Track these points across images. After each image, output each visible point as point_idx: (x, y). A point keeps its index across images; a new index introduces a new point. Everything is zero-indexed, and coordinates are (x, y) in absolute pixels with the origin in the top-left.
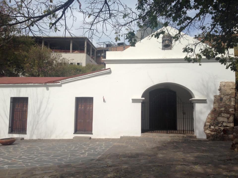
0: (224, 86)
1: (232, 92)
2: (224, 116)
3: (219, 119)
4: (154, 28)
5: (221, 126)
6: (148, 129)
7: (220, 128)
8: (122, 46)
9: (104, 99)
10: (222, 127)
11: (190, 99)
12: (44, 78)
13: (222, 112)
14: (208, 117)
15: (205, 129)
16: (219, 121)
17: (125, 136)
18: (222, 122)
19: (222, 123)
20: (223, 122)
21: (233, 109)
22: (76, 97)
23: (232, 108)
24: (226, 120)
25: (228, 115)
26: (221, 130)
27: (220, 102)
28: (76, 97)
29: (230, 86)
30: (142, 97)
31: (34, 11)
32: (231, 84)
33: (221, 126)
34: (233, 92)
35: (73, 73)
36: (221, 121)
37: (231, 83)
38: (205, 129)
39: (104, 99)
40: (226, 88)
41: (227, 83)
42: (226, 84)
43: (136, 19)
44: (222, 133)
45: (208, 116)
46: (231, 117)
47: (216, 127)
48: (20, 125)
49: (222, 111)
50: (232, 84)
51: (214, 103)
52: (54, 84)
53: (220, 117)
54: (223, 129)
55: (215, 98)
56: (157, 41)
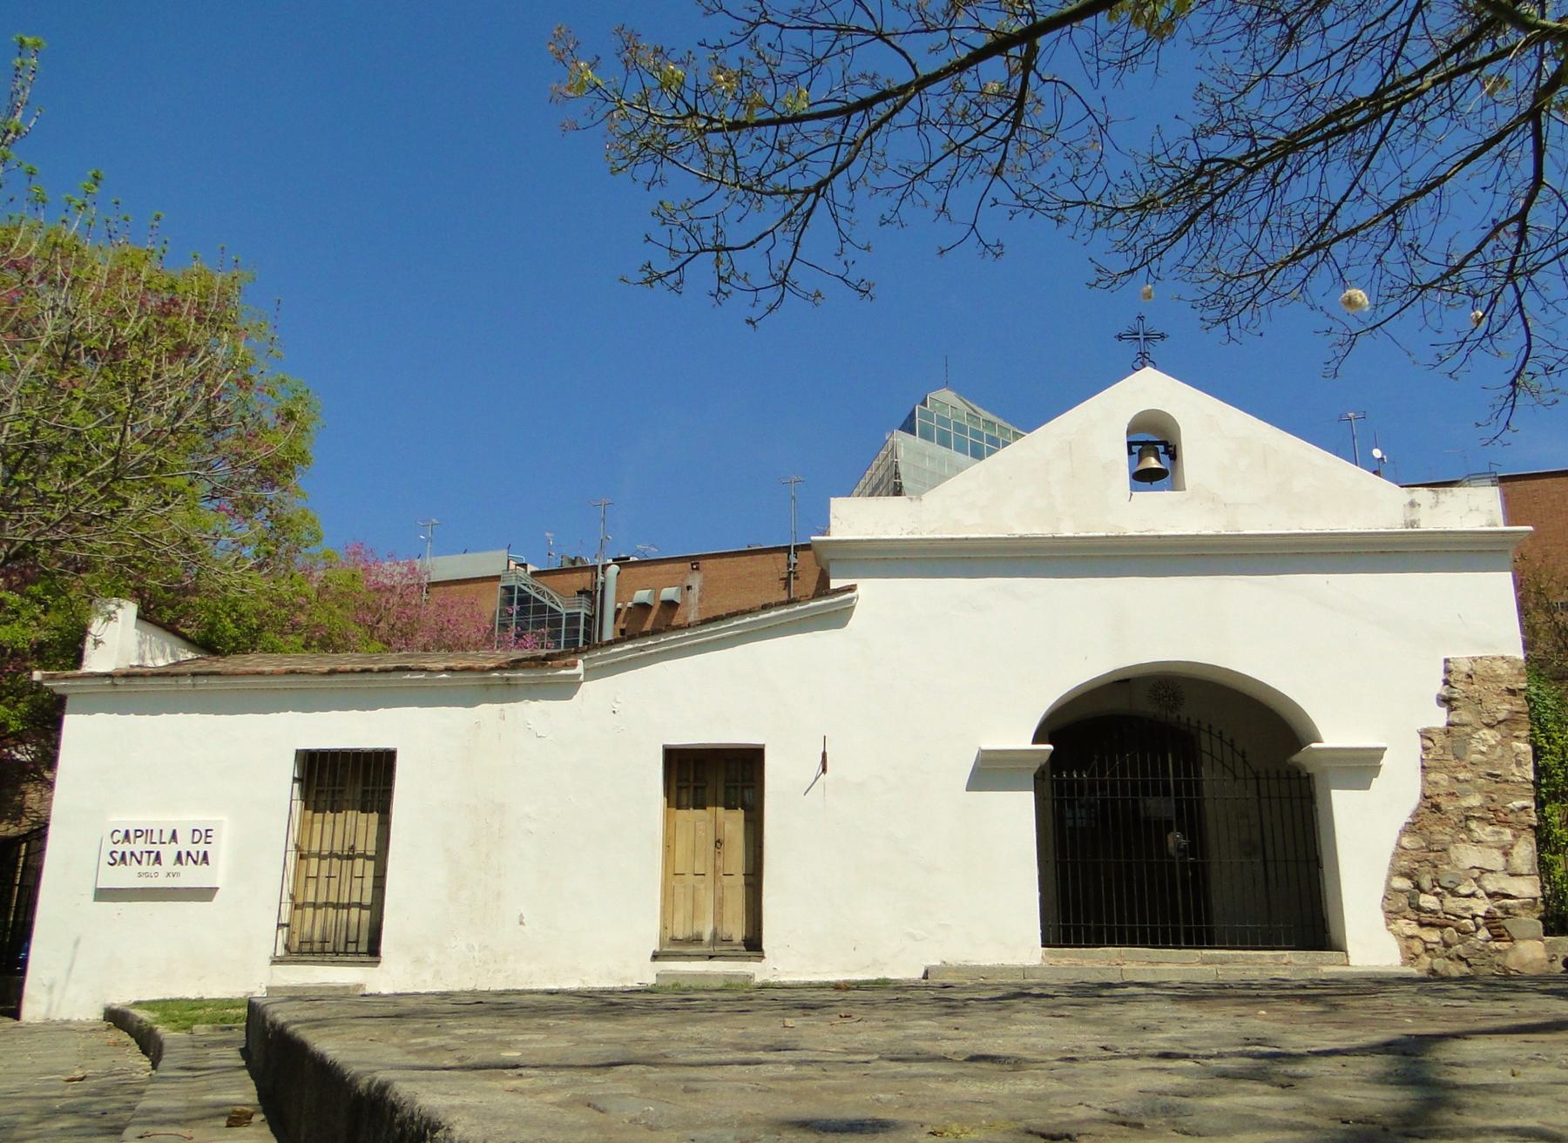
1: (1510, 712)
2: (1484, 837)
5: (1473, 895)
7: (1472, 902)
10: (1481, 902)
11: (1170, 755)
14: (1399, 845)
15: (1390, 912)
20: (1483, 871)
21: (1526, 803)
22: (298, 752)
23: (1523, 797)
24: (1495, 860)
25: (1507, 834)
26: (1474, 917)
28: (298, 752)
29: (1497, 678)
30: (1036, 741)
31: (1328, 28)
32: (1502, 669)
33: (1473, 895)
34: (1515, 708)
35: (262, 598)
37: (1500, 663)
38: (1390, 912)
42: (1478, 668)
44: (1484, 934)
45: (1399, 839)
46: (1521, 842)
48: (1338, 992)
49: (1469, 809)
51: (1423, 767)
52: (620, 649)
54: (1485, 908)
55: (47, 775)
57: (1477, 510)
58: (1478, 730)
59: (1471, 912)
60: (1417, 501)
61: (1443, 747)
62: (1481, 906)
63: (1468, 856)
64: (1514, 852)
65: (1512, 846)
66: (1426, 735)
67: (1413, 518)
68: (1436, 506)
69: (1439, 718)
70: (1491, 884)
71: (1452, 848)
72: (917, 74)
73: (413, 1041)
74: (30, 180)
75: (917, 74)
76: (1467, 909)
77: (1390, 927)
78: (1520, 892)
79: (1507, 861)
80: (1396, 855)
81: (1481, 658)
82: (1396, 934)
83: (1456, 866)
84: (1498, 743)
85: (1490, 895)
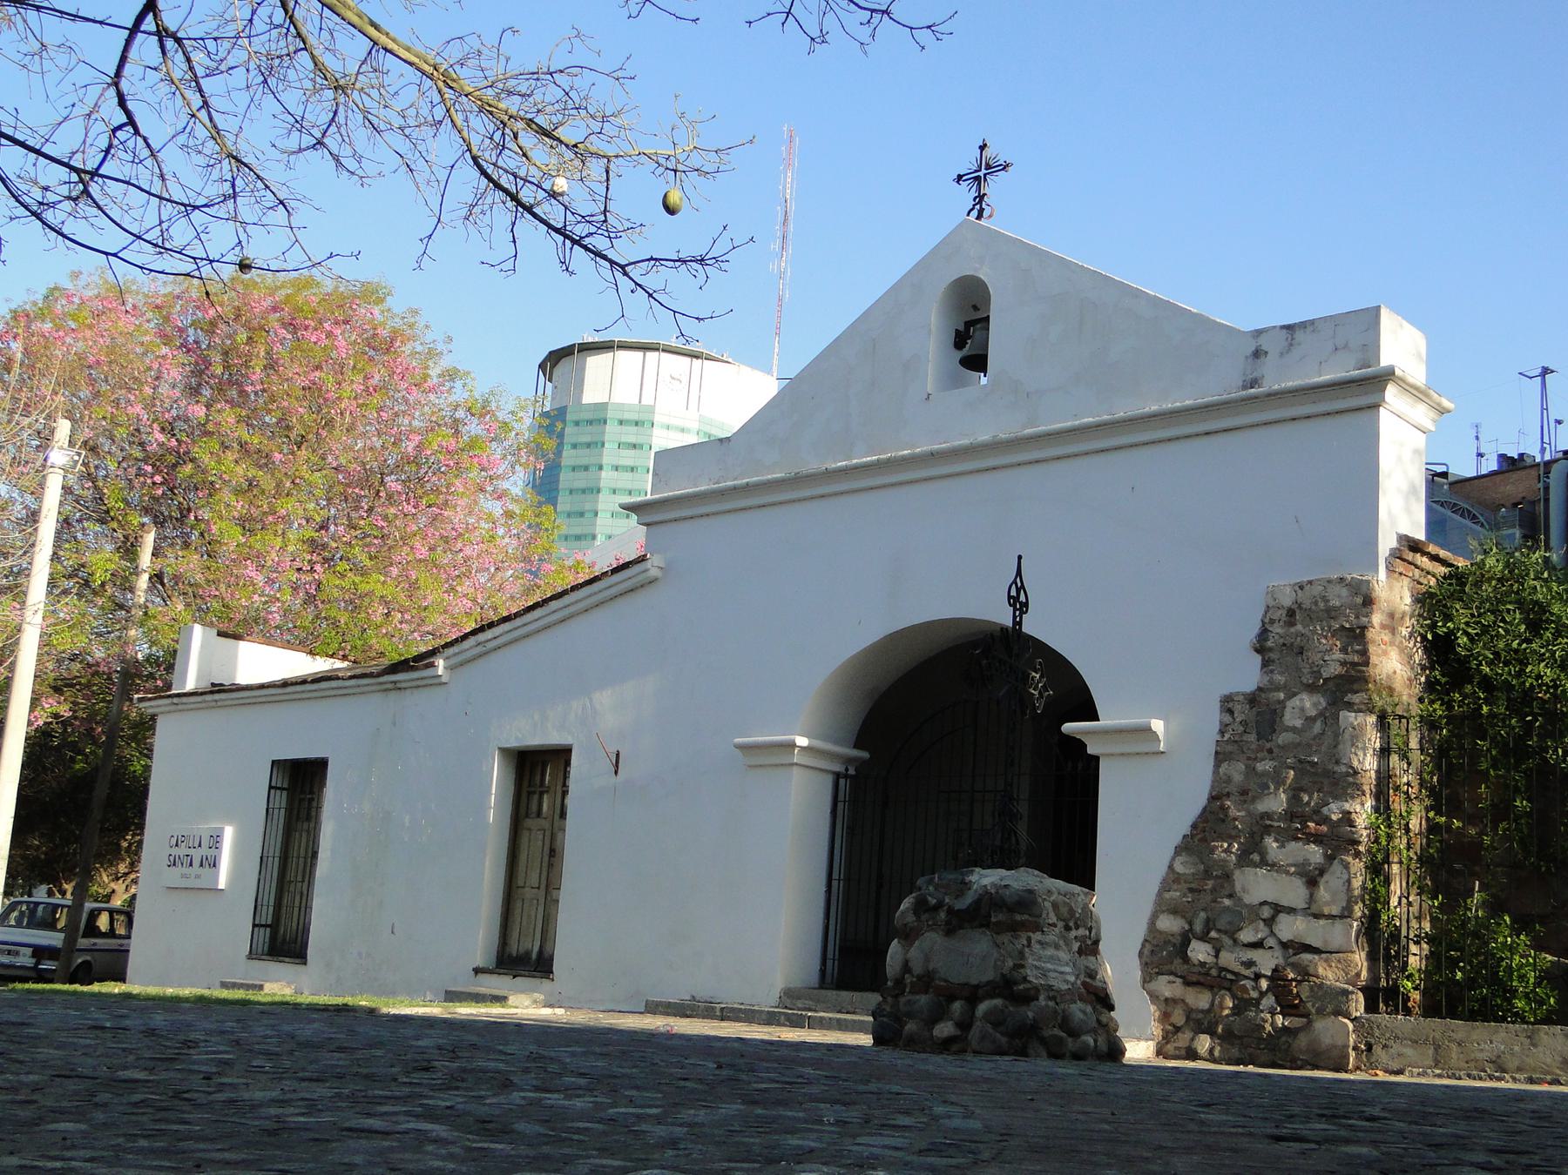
0: (1291, 613)
3: (1244, 890)
4: (1349, 703)
5: (1258, 945)
6: (817, 986)
8: (266, 949)
9: (697, 318)
10: (1269, 953)
12: (24, 734)
13: (1267, 830)
14: (1171, 867)
16: (1247, 900)
17: (749, 369)
18: (1266, 912)
19: (1270, 922)
20: (1278, 909)
24: (1292, 892)
26: (1258, 976)
27: (1260, 749)
33: (1258, 945)
36: (1265, 903)
39: (697, 318)
40: (1299, 627)
41: (1307, 588)
43: (150, 16)
45: (1173, 859)
47: (1223, 954)
50: (1344, 592)
53: (1256, 866)
55: (1228, 719)
56: (1020, 558)
57: (1346, 346)
58: (1295, 695)
59: (1253, 969)
60: (1264, 348)
61: (1244, 723)
62: (1267, 962)
63: (1257, 886)
64: (1322, 881)
65: (1322, 872)
66: (1227, 703)
67: (1255, 374)
68: (1289, 351)
69: (1247, 675)
70: (1290, 928)
71: (1237, 874)
72: (37, 159)
73: (231, 1056)
74: (866, 53)
75: (37, 159)
76: (1250, 964)
77: (1152, 986)
78: (1326, 942)
79: (1311, 895)
80: (1165, 886)
81: (1310, 582)
82: (1154, 997)
83: (1240, 899)
84: (1321, 714)
85: (1285, 945)
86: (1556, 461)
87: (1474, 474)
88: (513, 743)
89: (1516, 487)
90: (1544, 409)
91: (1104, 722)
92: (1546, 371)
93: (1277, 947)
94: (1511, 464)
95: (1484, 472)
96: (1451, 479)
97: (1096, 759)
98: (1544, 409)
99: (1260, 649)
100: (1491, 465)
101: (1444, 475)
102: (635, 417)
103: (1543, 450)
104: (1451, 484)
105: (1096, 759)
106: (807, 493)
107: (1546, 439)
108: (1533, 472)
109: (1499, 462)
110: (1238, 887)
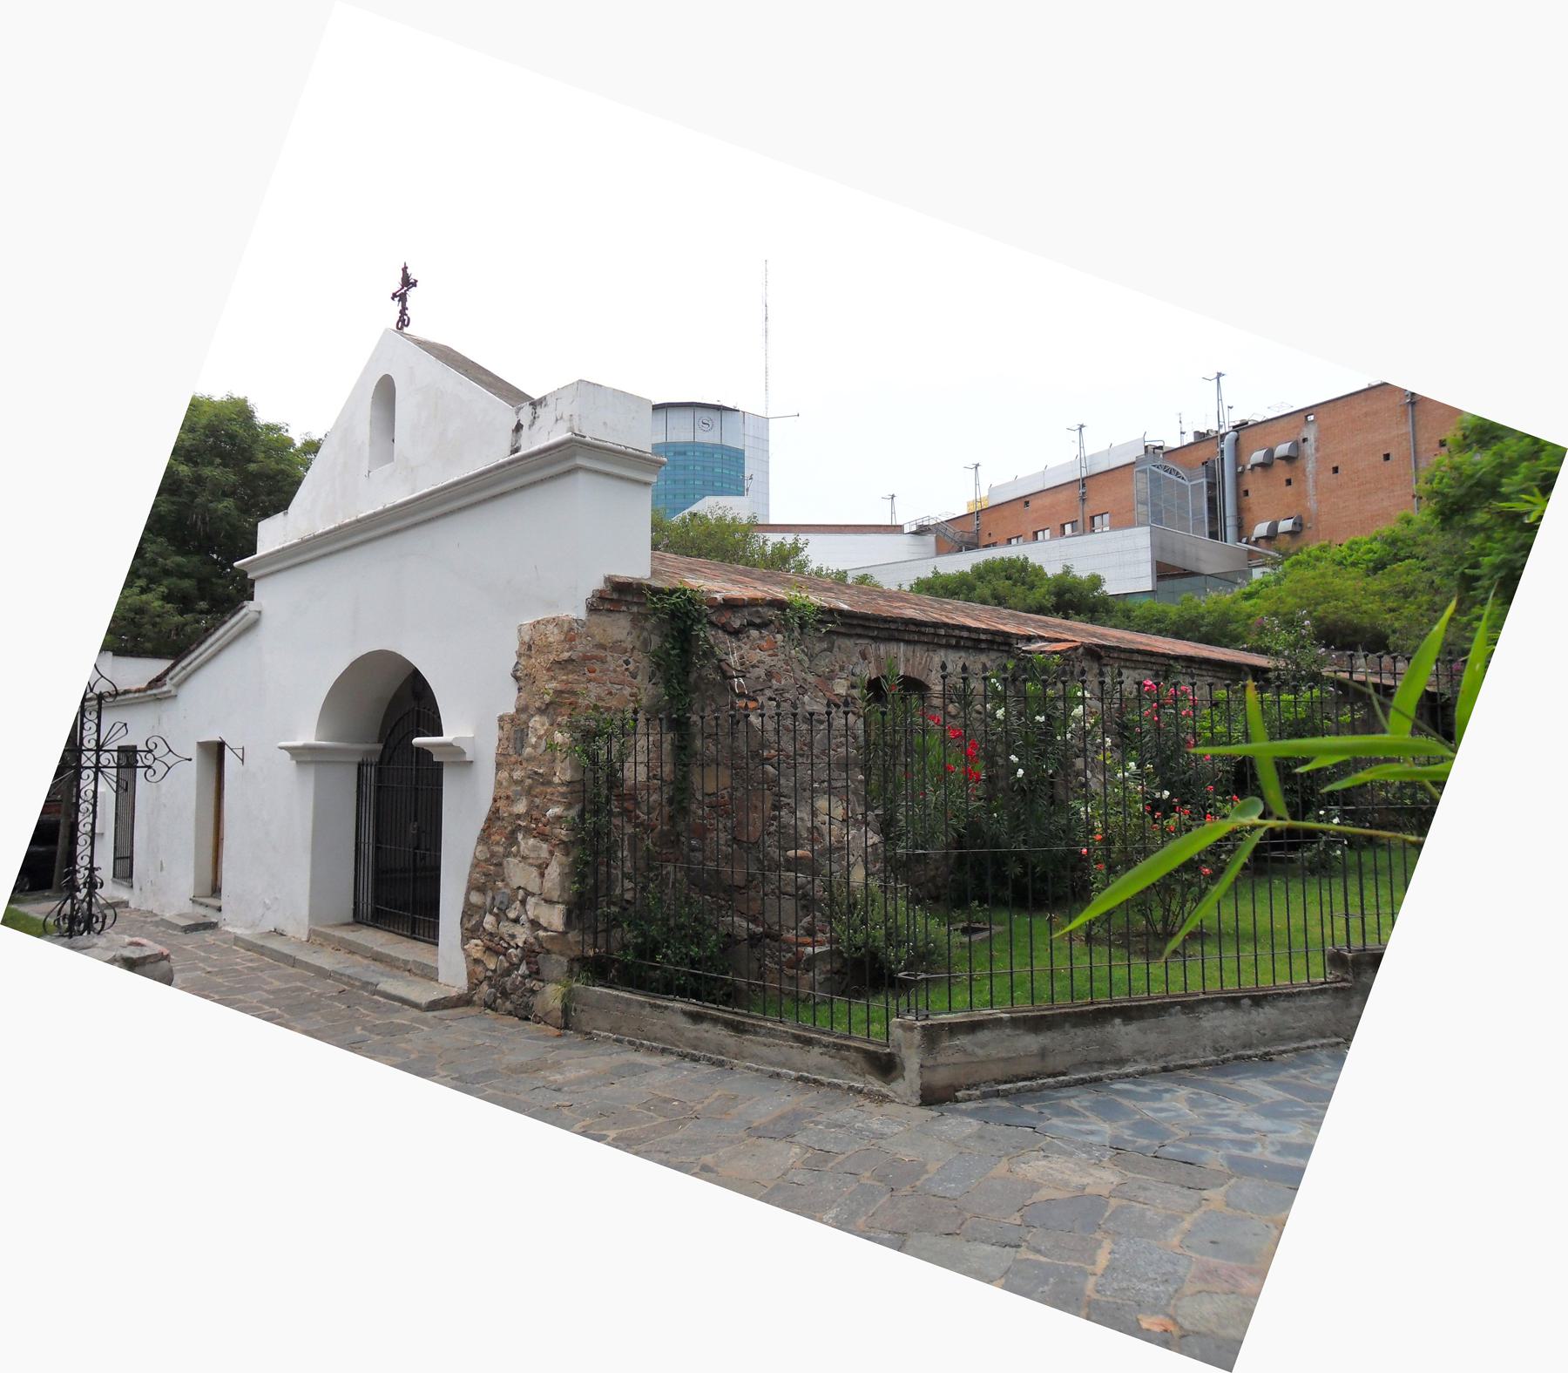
36: (519, 888)
86: (1227, 433)
87: (1179, 446)
88: (202, 740)
89: (1205, 452)
90: (1219, 400)
91: (447, 737)
92: (1219, 375)
93: (527, 925)
94: (1201, 437)
95: (1185, 444)
96: (1165, 450)
97: (440, 764)
98: (1219, 400)
99: (517, 679)
100: (1190, 439)
101: (1161, 448)
102: (682, 449)
103: (1220, 426)
104: (1164, 453)
105: (440, 764)
106: (307, 557)
107: (1221, 419)
108: (1214, 441)
109: (1195, 437)
110: (506, 875)
